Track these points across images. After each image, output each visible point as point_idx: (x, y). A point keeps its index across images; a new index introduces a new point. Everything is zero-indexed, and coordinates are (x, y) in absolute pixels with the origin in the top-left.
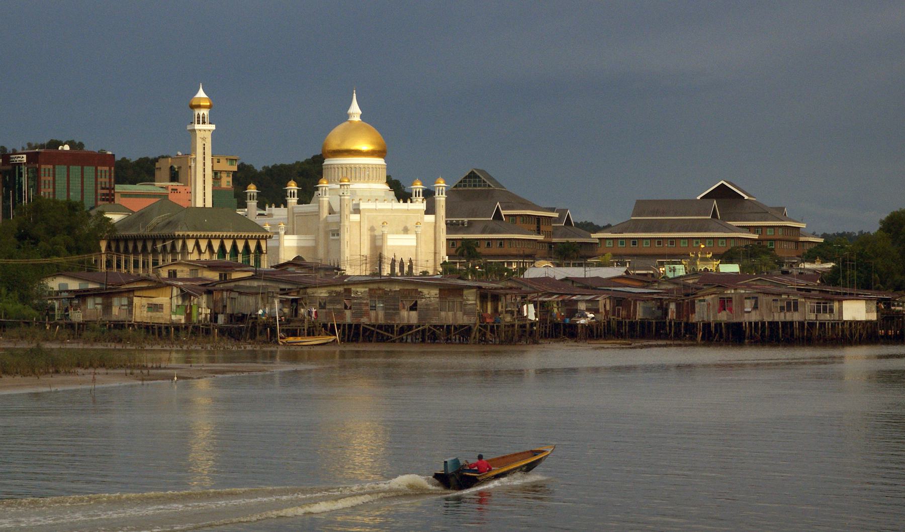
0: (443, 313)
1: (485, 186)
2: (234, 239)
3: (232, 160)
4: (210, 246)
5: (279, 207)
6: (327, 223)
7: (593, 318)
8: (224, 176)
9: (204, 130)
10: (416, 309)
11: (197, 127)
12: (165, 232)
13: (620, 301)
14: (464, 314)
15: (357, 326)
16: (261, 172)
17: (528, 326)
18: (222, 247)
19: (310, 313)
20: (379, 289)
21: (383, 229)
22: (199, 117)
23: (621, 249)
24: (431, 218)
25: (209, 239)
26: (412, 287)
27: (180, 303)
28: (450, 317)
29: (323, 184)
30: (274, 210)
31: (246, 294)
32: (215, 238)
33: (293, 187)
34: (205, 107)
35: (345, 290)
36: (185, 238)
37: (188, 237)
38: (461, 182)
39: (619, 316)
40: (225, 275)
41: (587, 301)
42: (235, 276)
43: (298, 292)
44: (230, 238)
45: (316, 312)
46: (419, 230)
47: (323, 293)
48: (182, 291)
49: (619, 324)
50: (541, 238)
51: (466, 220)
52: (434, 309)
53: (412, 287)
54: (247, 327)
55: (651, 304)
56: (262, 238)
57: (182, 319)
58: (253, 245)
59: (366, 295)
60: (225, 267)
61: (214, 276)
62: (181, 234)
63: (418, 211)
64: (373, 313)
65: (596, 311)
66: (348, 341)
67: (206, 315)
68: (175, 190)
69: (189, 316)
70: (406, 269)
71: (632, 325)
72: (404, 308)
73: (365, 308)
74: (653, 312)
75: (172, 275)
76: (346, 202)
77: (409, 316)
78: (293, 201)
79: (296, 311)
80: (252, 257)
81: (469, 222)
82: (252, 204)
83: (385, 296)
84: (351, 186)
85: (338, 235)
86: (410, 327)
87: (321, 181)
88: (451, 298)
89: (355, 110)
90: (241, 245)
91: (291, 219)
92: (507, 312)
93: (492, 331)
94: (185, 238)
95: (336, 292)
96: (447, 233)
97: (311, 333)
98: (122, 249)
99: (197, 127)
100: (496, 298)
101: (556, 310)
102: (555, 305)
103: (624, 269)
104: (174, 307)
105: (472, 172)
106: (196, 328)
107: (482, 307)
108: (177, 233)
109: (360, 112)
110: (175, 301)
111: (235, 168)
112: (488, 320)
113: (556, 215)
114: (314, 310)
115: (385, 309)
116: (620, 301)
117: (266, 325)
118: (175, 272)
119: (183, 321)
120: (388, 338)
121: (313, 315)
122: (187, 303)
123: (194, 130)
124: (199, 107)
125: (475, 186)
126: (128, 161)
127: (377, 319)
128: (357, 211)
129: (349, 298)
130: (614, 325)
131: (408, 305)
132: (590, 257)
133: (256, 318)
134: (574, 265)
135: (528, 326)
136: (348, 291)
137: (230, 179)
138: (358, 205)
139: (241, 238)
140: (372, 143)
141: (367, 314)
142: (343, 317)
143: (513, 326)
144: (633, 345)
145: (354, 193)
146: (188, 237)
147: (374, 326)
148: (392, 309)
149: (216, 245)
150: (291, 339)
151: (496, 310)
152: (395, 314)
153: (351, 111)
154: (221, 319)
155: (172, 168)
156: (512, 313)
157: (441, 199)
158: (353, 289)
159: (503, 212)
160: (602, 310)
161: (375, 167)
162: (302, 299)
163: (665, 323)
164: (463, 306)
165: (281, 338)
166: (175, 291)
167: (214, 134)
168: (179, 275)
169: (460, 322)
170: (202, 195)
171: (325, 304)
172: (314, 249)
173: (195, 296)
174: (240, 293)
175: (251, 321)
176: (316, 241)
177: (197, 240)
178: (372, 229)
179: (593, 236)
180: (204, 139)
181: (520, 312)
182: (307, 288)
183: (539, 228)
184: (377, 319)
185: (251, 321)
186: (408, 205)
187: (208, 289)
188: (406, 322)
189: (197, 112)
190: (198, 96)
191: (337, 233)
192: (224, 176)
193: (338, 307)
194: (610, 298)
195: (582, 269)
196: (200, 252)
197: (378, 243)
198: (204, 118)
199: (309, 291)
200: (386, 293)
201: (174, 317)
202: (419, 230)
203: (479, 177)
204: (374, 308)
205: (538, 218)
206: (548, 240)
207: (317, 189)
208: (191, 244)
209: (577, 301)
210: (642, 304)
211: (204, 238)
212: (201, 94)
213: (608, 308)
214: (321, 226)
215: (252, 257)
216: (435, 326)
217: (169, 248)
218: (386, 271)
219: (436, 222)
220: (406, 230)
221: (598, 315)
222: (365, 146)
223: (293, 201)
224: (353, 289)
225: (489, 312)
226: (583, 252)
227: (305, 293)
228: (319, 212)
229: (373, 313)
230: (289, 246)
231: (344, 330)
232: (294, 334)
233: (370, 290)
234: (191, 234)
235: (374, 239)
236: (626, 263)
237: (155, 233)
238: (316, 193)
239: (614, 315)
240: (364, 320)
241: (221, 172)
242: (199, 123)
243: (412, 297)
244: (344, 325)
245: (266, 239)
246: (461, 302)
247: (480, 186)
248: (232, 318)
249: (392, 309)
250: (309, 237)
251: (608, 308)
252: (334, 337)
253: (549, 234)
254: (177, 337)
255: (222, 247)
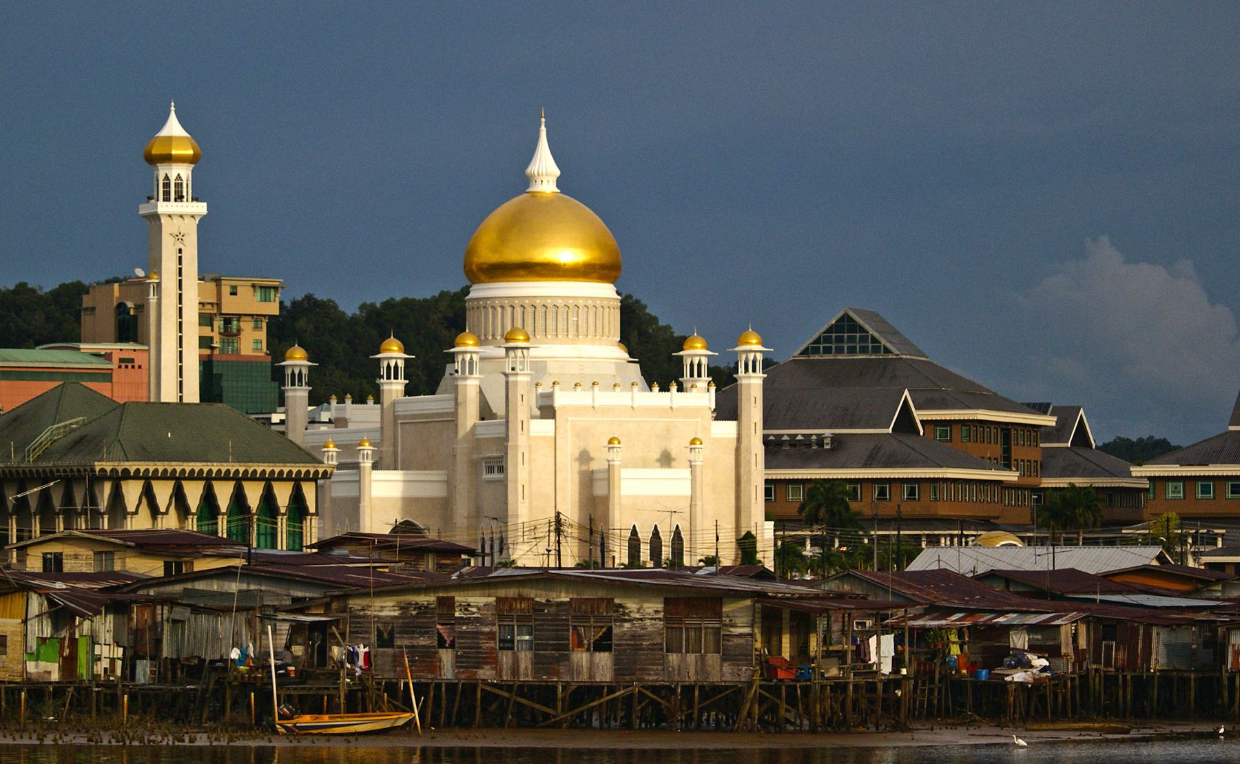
0: (673, 658)
1: (876, 350)
2: (238, 481)
3: (265, 288)
4: (179, 497)
5: (364, 402)
6: (476, 442)
7: (1044, 669)
8: (247, 326)
9: (181, 217)
10: (607, 648)
11: (163, 207)
12: (72, 462)
13: (1111, 627)
14: (724, 660)
15: (471, 687)
16: (354, 319)
17: (880, 686)
18: (209, 498)
19: (352, 657)
20: (521, 598)
21: (611, 456)
22: (167, 185)
23: (1203, 501)
24: (728, 428)
25: (178, 480)
26: (601, 594)
27: (47, 632)
28: (685, 666)
29: (468, 347)
30: (351, 409)
31: (209, 611)
32: (192, 477)
33: (393, 353)
34: (182, 160)
35: (440, 600)
36: (118, 478)
37: (126, 476)
38: (818, 341)
39: (1108, 664)
40: (179, 566)
41: (1031, 629)
42: (200, 565)
43: (327, 607)
44: (226, 477)
45: (367, 655)
46: (699, 458)
47: (386, 608)
48: (51, 603)
49: (1110, 681)
50: (1011, 476)
51: (828, 432)
52: (656, 647)
53: (601, 594)
54: (205, 691)
55: (1187, 637)
56: (307, 478)
57: (53, 671)
58: (283, 494)
59: (489, 615)
60: (179, 546)
61: (154, 567)
62: (108, 466)
63: (693, 412)
64: (506, 658)
65: (1052, 652)
66: (448, 724)
67: (112, 661)
68: (126, 362)
69: (69, 664)
70: (666, 552)
71: (1142, 684)
72: (580, 645)
73: (487, 645)
74: (1194, 653)
75: (53, 566)
76: (521, 390)
77: (591, 663)
78: (394, 388)
79: (323, 652)
80: (282, 524)
81: (835, 438)
82: (298, 394)
83: (533, 617)
84: (532, 352)
85: (502, 469)
86: (593, 690)
87: (385, 344)
88: (692, 621)
89: (545, 169)
90: (253, 494)
91: (388, 433)
92: (828, 654)
93: (792, 700)
94: (118, 478)
95: (418, 607)
96: (768, 466)
97: (357, 703)
98: (103, 504)
99: (163, 207)
100: (803, 623)
101: (955, 650)
102: (954, 638)
103: (1157, 550)
104: (33, 644)
105: (846, 317)
106: (83, 691)
107: (767, 642)
108: (98, 466)
109: (558, 172)
110: (34, 627)
111: (273, 309)
112: (781, 674)
113: (1050, 421)
114: (362, 650)
115: (534, 646)
116: (1111, 627)
117: (246, 685)
118: (58, 558)
119: (55, 677)
120: (546, 716)
121: (361, 662)
122: (64, 633)
123: (156, 217)
124: (168, 159)
125: (852, 350)
126: (33, 291)
127: (591, 674)
128: (547, 411)
129: (450, 621)
130: (1096, 684)
131: (593, 635)
132: (1128, 524)
133: (225, 669)
134: (1090, 542)
135: (880, 686)
136: (447, 604)
137: (262, 335)
138: (550, 396)
139: (253, 478)
140: (584, 246)
141: (491, 659)
142: (435, 666)
143: (844, 687)
144: (1134, 734)
145: (539, 368)
146: (126, 476)
147: (509, 688)
148: (552, 650)
149: (194, 493)
150: (306, 720)
151: (801, 649)
152: (558, 660)
153: (533, 168)
154: (144, 671)
155: (121, 307)
156: (841, 655)
157: (752, 384)
158: (459, 598)
159: (919, 415)
160: (1066, 649)
161: (594, 305)
162: (336, 623)
163: (1220, 679)
164: (721, 642)
165: (282, 717)
166: (36, 604)
167: (204, 225)
168: (69, 566)
169: (715, 678)
170: (176, 372)
171: (391, 634)
172: (445, 505)
173: (83, 616)
174: (196, 610)
175: (214, 677)
176: (450, 483)
177: (148, 480)
178: (584, 457)
179: (1136, 471)
180: (179, 237)
181: (861, 653)
182: (346, 596)
183: (1007, 451)
184: (515, 669)
185: (214, 677)
186: (673, 397)
187: (118, 597)
188: (584, 677)
189: (163, 170)
190: (164, 132)
191: (499, 465)
192: (247, 326)
193: (423, 641)
194: (1086, 620)
195: (642, 546)
196: (155, 511)
197: (599, 490)
198: (179, 186)
199: (355, 604)
200: (537, 608)
201: (31, 667)
202: (699, 458)
203: (862, 330)
204: (508, 644)
205: (1006, 428)
206: (1030, 481)
207: (452, 358)
208: (132, 492)
209: (1008, 628)
210: (1164, 634)
211: (165, 477)
212: (173, 128)
213: (1082, 643)
214: (461, 448)
215: (282, 524)
216: (655, 689)
217: (33, 504)
218: (620, 555)
219: (739, 439)
220: (666, 460)
221: (1056, 661)
222: (568, 253)
223: (394, 388)
224: (459, 598)
225: (786, 654)
226: (1118, 513)
227: (344, 609)
228: (455, 414)
229: (506, 658)
230: (384, 498)
231: (437, 698)
232: (316, 708)
233: (499, 600)
234: (132, 467)
235: (588, 480)
236: (1216, 536)
237: (47, 464)
238: (449, 368)
239: (1097, 660)
240: (486, 673)
241: (239, 316)
242: (167, 199)
243: (600, 618)
244: (438, 686)
245: (315, 479)
246: (717, 632)
247: (864, 350)
248: (169, 669)
249: (552, 650)
250: (436, 475)
251: (1082, 643)
252: (406, 717)
253: (1029, 468)
254: (35, 715)
255: (209, 498)
